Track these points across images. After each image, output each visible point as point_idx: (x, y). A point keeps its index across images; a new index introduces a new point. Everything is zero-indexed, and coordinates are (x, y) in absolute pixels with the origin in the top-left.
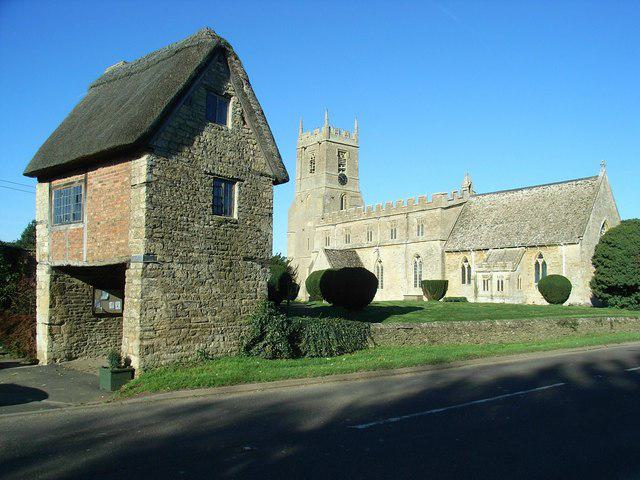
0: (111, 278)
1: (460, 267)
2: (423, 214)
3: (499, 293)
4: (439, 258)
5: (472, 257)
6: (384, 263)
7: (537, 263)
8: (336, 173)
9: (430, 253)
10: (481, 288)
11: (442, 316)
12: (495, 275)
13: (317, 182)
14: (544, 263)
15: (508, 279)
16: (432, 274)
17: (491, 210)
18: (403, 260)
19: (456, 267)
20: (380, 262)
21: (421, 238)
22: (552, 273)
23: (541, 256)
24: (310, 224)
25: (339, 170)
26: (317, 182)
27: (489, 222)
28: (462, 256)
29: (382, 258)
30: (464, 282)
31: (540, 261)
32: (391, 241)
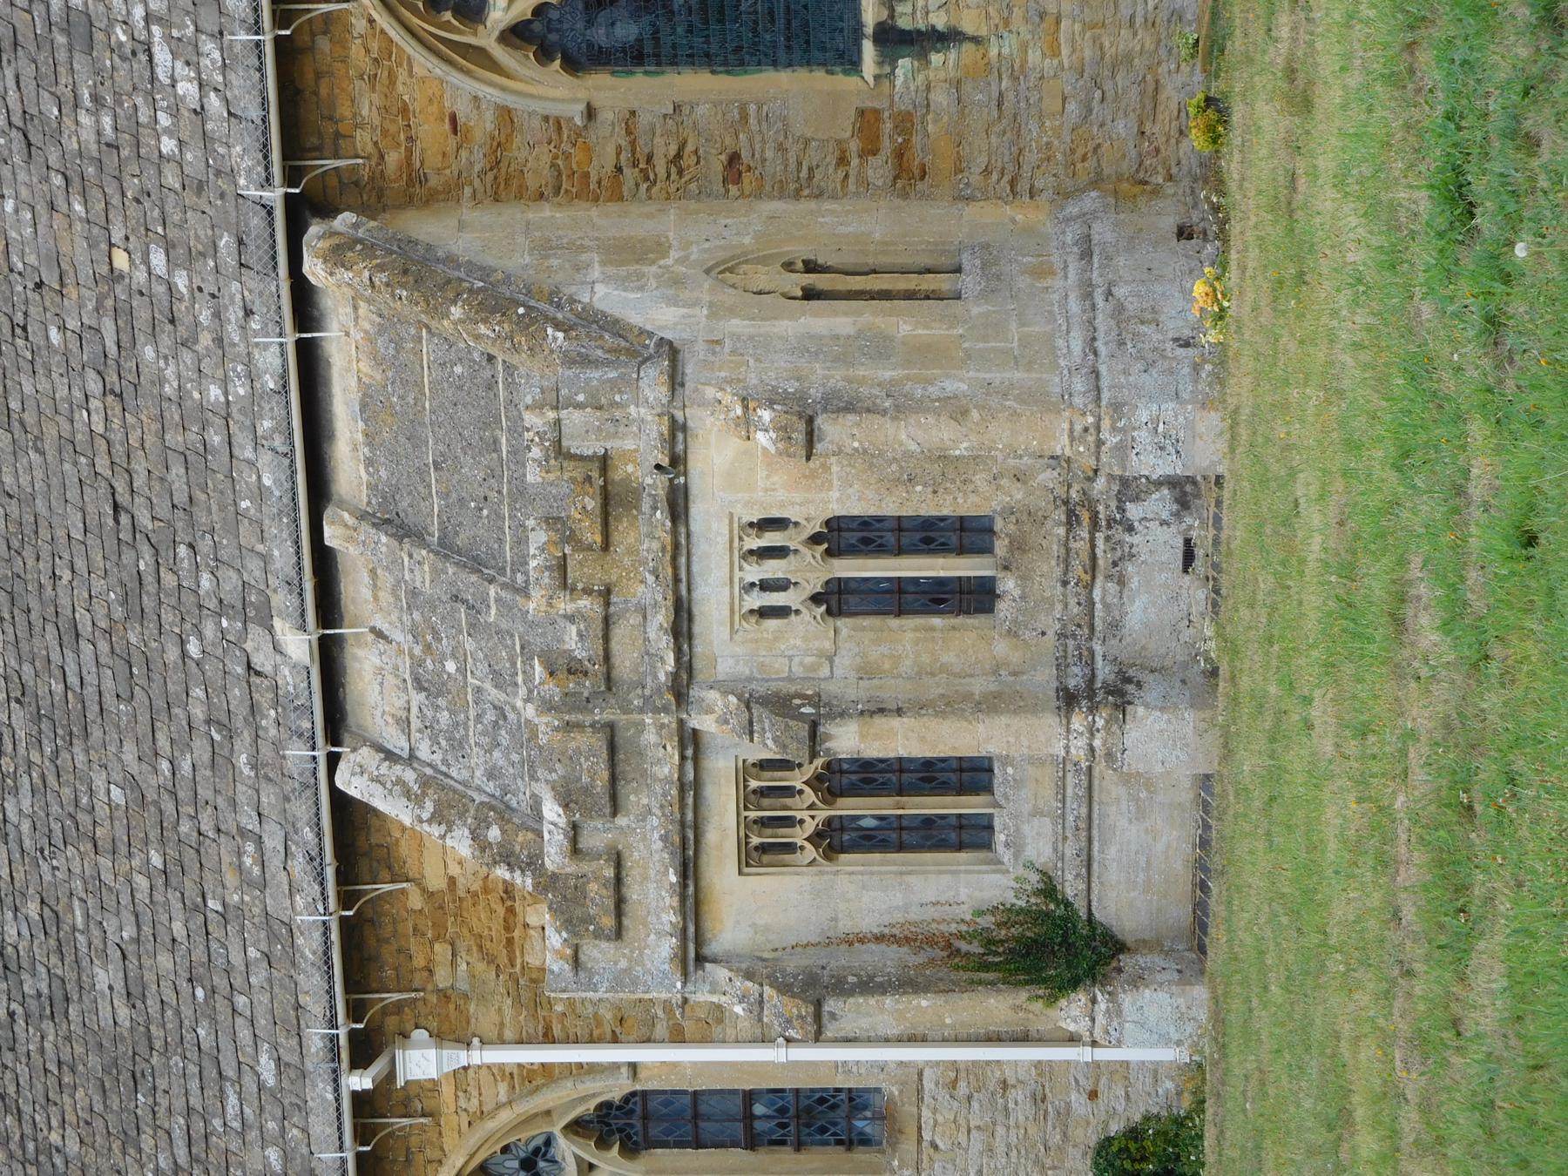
3: (1032, 592)
12: (725, 644)
15: (805, 430)
31: (811, 570)
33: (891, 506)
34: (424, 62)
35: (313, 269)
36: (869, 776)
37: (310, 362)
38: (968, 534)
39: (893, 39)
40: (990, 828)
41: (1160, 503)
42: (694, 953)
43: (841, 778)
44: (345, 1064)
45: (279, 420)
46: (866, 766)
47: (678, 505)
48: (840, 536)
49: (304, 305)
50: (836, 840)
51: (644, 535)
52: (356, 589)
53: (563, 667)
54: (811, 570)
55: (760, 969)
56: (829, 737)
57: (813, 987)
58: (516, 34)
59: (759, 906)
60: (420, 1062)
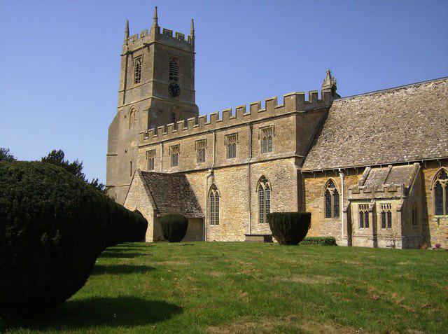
0: (360, 205)
2: (271, 123)
4: (295, 182)
5: (339, 181)
6: (220, 189)
7: (327, 192)
8: (166, 83)
9: (281, 176)
10: (356, 223)
11: (438, 252)
12: (378, 203)
13: (143, 93)
14: (336, 194)
16: (285, 204)
17: (363, 116)
18: (245, 186)
19: (318, 195)
20: (216, 189)
21: (268, 155)
22: (279, 211)
24: (134, 144)
25: (171, 78)
26: (143, 93)
27: (362, 130)
28: (325, 180)
29: (218, 183)
30: (328, 215)
31: (386, 211)
32: (230, 161)
33: (392, 219)
34: (435, 174)
35: (415, 164)
36: (367, 216)
37: (406, 164)
38: (390, 226)
39: (438, 219)
40: (177, 165)
41: (393, 244)
42: (351, 201)
43: (367, 213)
44: (141, 244)
45: (400, 161)
46: (368, 216)
47: (392, 199)
48: (389, 213)
49: (412, 163)
50: (361, 213)
52: (385, 169)
53: (377, 188)
54: (386, 211)
55: (349, 206)
56: (68, 162)
57: (348, 211)
58: (438, 182)
59: (355, 206)
60: (341, 175)
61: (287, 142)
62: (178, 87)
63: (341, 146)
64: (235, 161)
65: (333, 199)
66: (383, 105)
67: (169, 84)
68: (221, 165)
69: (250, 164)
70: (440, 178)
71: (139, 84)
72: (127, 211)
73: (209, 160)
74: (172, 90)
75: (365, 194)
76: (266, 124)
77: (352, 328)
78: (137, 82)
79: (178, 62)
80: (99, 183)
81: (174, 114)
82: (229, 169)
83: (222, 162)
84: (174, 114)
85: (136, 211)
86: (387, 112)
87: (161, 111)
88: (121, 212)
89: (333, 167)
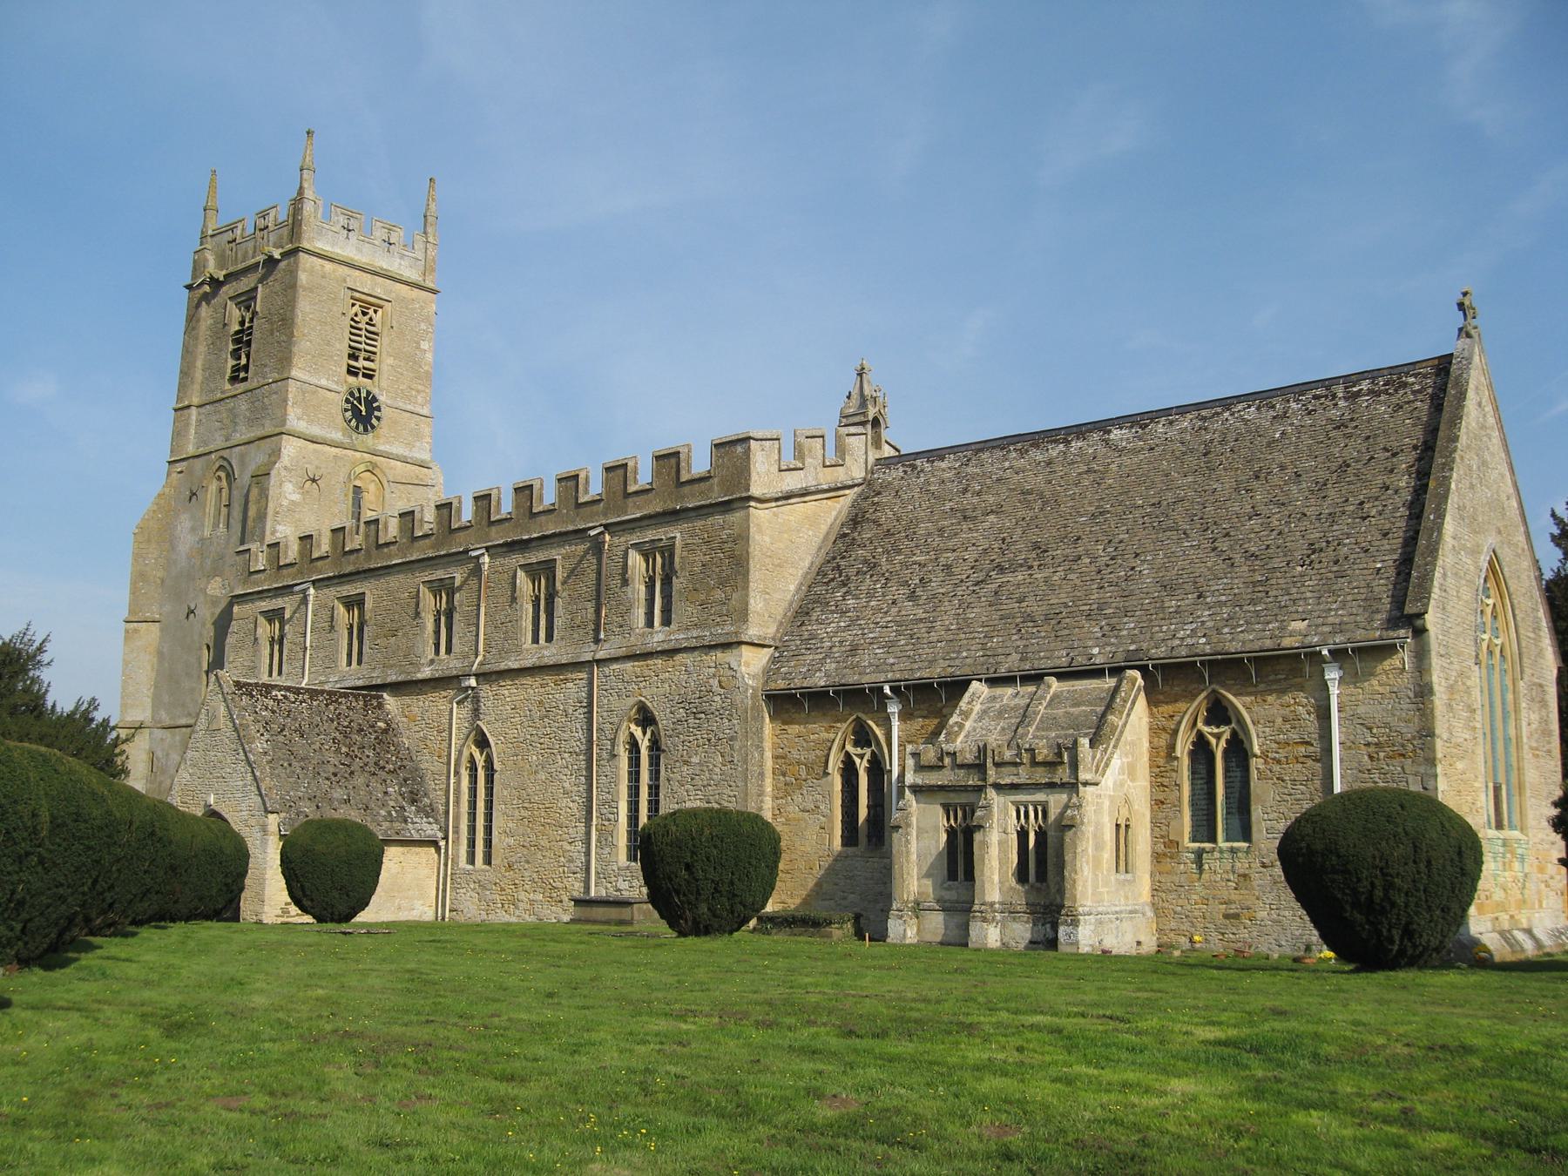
1: (835, 763)
23: (1219, 713)
39: (1199, 854)
47: (1051, 786)
51: (1041, 776)
60: (893, 709)
61: (719, 594)
62: (375, 399)
63: (894, 610)
64: (550, 653)
65: (481, 774)
66: (1036, 481)
67: (344, 389)
68: (503, 666)
69: (599, 662)
70: (1208, 722)
71: (241, 387)
72: (184, 816)
73: (474, 647)
74: (356, 412)
75: (962, 772)
76: (650, 535)
77: (977, 837)
78: (234, 379)
79: (377, 319)
80: (99, 716)
81: (357, 490)
82: (528, 681)
83: (504, 653)
84: (357, 490)
85: (213, 814)
86: (1045, 503)
87: (314, 480)
88: (154, 825)
89: (868, 679)
